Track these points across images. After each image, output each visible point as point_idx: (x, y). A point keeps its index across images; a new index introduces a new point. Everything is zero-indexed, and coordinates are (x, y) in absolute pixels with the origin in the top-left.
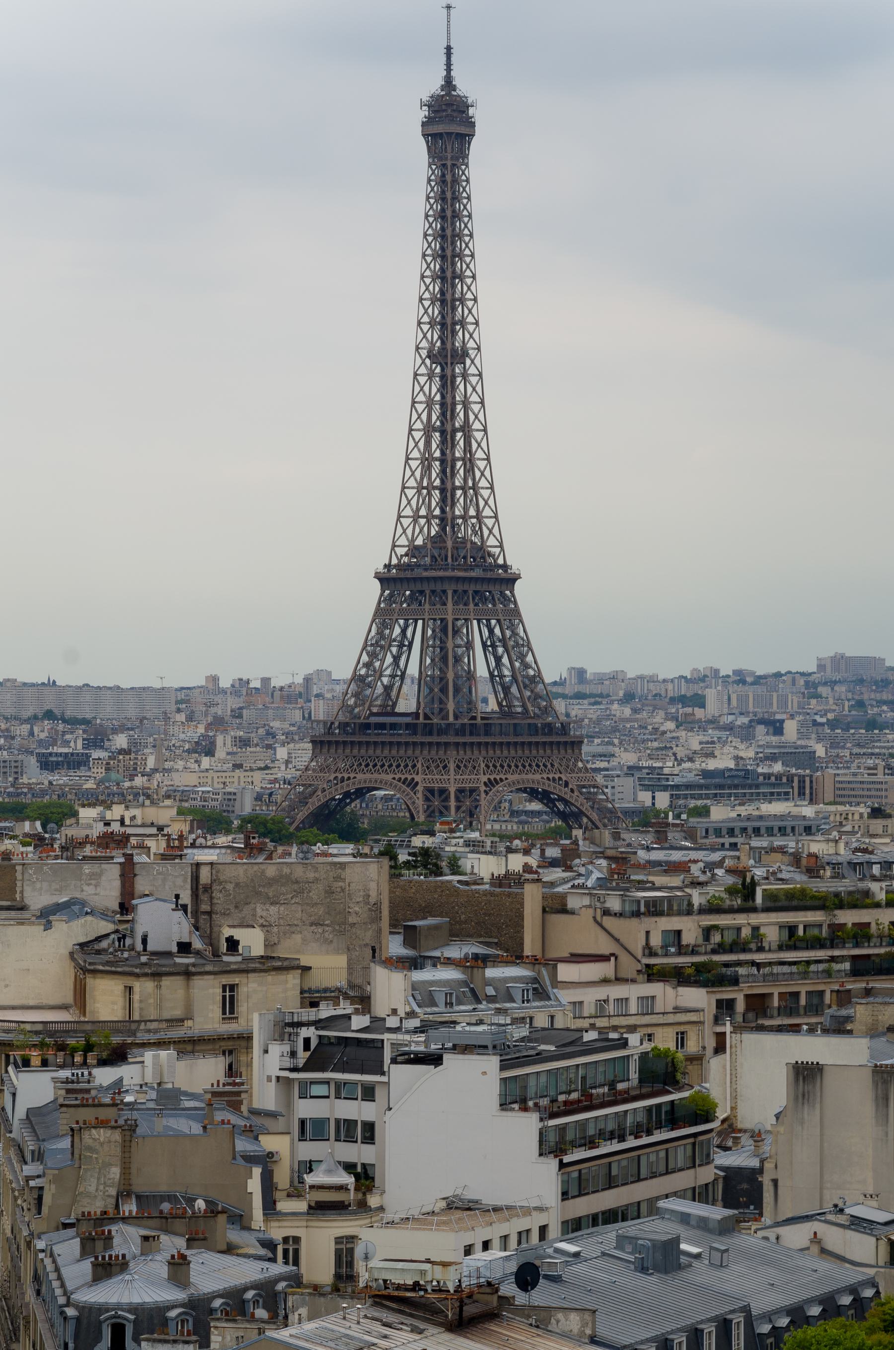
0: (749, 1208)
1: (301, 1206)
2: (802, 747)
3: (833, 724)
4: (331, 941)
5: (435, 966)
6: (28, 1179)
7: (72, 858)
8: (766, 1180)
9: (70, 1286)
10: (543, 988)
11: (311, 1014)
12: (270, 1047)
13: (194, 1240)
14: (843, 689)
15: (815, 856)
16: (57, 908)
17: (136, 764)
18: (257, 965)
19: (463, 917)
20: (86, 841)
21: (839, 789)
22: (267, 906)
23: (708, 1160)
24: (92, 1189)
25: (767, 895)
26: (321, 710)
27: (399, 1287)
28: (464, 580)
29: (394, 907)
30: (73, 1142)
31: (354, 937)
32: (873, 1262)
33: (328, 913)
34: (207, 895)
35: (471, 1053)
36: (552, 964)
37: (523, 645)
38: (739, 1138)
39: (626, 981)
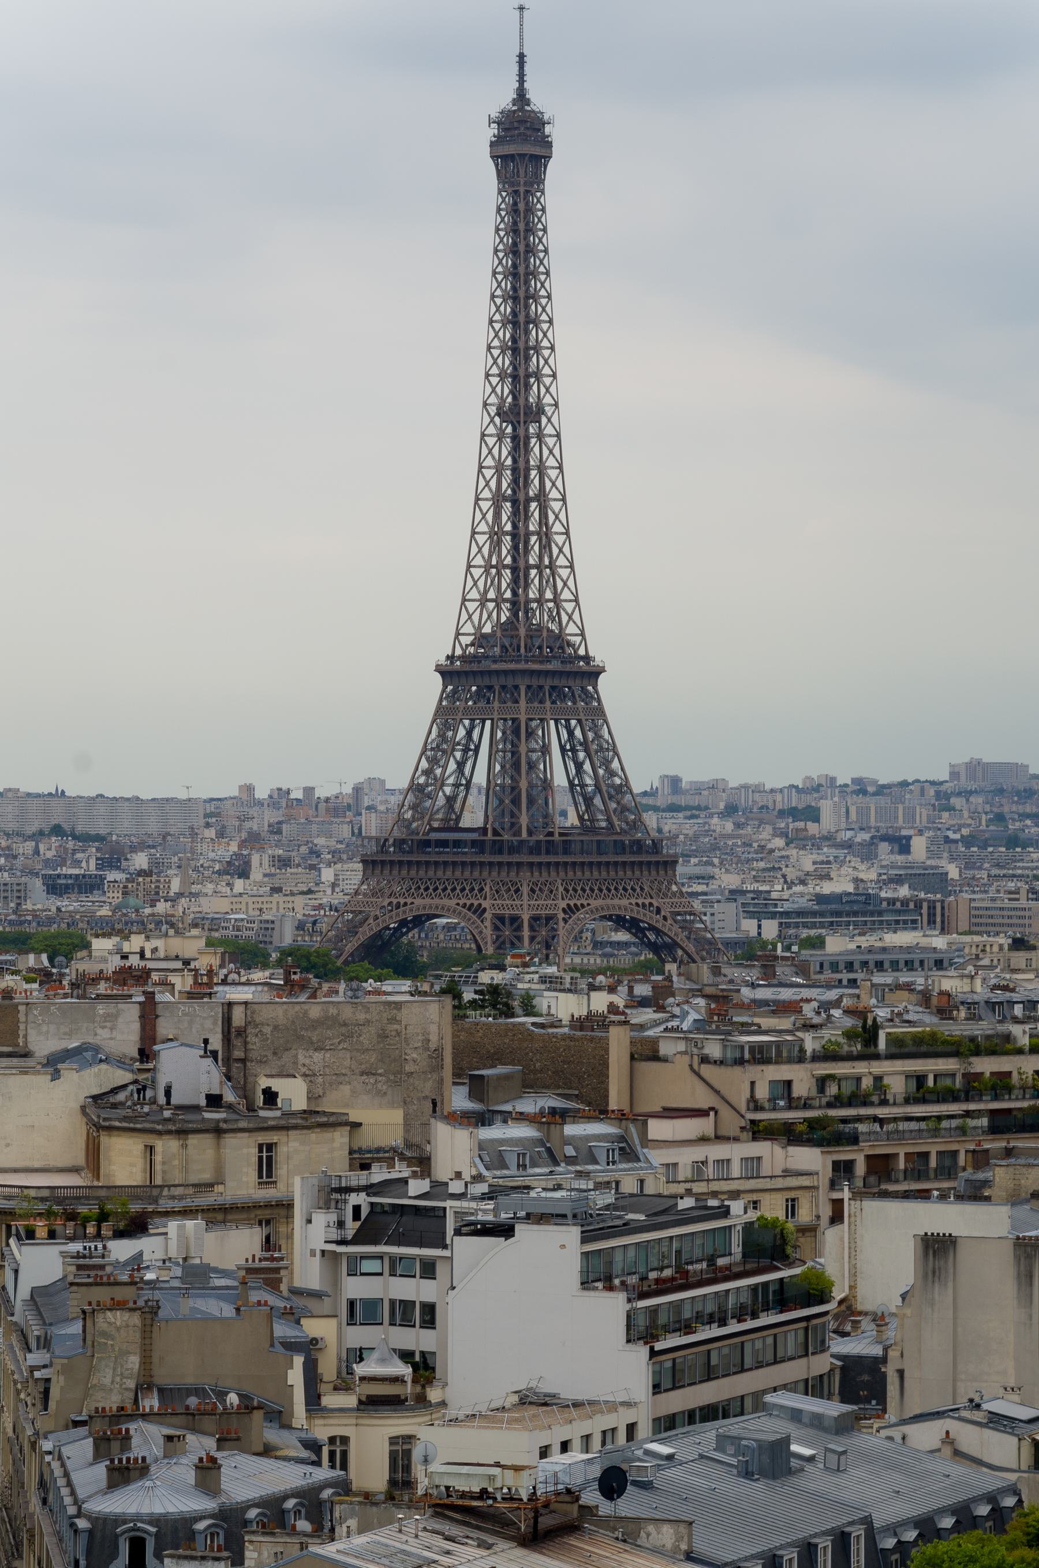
0: (870, 1403)
1: (350, 1401)
2: (932, 867)
3: (968, 841)
4: (385, 1093)
5: (505, 1121)
6: (32, 1369)
7: (83, 996)
8: (890, 1370)
9: (81, 1494)
10: (631, 1148)
11: (361, 1178)
12: (314, 1216)
13: (226, 1440)
14: (980, 800)
15: (947, 994)
16: (67, 1055)
17: (158, 887)
18: (299, 1121)
19: (538, 1065)
20: (100, 977)
21: (975, 916)
22: (311, 1052)
23: (822, 1347)
24: (107, 1381)
25: (892, 1040)
26: (373, 825)
27: (463, 1495)
28: (539, 673)
29: (458, 1053)
30: (84, 1326)
31: (411, 1088)
32: (1015, 1466)
33: (382, 1061)
34: (240, 1040)
35: (548, 1223)
36: (641, 1120)
37: (608, 750)
38: (859, 1322)
39: (727, 1139)
